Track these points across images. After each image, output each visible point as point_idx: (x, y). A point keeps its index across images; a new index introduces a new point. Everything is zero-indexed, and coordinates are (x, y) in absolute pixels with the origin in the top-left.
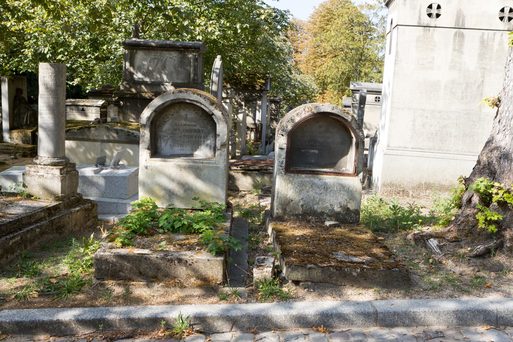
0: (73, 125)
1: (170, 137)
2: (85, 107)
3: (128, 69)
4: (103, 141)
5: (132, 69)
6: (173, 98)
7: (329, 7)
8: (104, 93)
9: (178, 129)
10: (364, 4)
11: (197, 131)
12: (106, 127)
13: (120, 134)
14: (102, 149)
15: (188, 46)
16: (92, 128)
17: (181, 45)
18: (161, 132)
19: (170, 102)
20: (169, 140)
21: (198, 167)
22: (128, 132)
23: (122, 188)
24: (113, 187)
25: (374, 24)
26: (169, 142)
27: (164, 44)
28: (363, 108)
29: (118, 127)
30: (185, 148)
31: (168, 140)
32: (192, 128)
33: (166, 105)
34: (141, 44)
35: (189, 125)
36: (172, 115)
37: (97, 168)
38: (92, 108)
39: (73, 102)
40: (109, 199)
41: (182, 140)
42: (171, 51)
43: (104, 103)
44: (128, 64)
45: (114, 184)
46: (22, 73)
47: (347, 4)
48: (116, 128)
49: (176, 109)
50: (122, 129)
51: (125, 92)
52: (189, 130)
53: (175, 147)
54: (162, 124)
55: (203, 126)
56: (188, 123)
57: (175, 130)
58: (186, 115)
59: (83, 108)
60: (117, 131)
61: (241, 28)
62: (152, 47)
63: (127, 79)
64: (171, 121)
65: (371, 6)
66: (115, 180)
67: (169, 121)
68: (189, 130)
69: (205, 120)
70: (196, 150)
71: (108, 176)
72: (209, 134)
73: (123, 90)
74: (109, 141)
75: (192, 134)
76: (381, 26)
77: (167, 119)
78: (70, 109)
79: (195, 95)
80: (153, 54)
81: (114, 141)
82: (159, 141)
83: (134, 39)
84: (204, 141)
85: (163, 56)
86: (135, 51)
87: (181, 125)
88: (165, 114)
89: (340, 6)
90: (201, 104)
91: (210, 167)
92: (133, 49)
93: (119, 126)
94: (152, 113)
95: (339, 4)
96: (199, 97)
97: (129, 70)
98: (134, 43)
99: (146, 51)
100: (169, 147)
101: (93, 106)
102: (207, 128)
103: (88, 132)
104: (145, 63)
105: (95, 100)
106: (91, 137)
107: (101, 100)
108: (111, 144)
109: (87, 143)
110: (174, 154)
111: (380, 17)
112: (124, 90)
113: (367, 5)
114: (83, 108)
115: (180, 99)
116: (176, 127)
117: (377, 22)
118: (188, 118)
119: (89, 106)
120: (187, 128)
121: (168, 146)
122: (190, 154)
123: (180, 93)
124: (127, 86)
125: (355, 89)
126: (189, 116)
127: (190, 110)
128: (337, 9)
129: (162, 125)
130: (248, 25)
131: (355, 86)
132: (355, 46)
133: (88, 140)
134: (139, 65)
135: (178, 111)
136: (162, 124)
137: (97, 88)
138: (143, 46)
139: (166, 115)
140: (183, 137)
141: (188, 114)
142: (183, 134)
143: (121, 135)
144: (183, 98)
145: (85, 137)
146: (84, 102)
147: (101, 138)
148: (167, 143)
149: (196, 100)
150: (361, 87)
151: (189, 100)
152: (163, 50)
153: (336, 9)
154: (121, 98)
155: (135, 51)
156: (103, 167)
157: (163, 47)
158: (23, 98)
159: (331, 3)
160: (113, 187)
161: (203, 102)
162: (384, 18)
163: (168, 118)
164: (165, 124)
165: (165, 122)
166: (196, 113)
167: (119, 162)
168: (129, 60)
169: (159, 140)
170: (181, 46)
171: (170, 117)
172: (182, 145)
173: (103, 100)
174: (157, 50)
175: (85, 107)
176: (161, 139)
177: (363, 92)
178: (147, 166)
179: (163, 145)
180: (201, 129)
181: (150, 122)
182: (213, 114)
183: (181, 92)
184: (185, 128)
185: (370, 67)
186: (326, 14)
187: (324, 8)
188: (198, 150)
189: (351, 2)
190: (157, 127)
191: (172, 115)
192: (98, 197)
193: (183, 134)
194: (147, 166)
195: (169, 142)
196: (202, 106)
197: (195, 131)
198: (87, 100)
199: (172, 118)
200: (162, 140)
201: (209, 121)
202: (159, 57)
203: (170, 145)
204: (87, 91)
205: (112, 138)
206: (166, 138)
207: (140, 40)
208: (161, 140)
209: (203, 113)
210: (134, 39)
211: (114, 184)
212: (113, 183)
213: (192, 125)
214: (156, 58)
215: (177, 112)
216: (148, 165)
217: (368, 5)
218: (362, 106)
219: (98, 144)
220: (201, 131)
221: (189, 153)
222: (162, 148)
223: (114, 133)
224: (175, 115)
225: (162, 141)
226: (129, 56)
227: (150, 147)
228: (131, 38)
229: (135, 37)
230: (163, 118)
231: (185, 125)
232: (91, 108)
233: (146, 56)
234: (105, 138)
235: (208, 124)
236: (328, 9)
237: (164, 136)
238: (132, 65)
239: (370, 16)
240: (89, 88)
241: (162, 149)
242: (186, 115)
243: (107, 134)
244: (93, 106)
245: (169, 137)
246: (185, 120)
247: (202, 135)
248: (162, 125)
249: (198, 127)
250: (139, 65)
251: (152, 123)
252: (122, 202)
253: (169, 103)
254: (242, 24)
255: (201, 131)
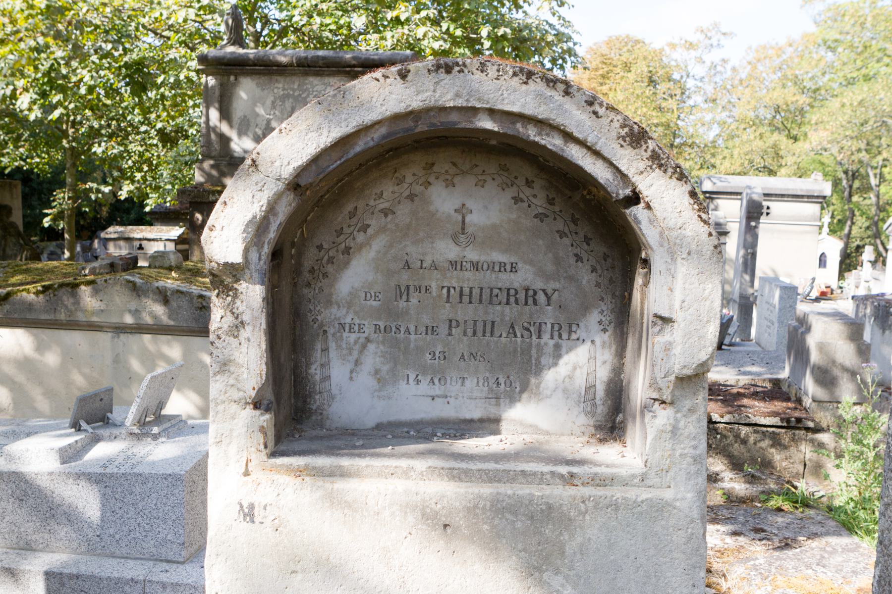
0: (29, 279)
1: (377, 328)
2: (144, 243)
3: (216, 126)
4: (120, 329)
5: (225, 128)
6: (400, 108)
7: (604, 53)
8: (183, 214)
9: (418, 289)
10: (676, 41)
11: (522, 296)
12: (129, 281)
13: (174, 304)
14: (118, 355)
15: (373, 60)
16: (83, 287)
17: (354, 58)
18: (329, 303)
19: (383, 130)
20: (371, 347)
21: (550, 507)
22: (201, 296)
23: (165, 520)
24: (131, 513)
25: (696, 77)
26: (372, 358)
27: (310, 56)
28: (756, 227)
29: (171, 282)
30: (454, 388)
31: (364, 347)
32: (490, 278)
33: (359, 146)
34: (249, 59)
35: (476, 266)
36: (385, 212)
37: (77, 438)
38: (160, 242)
39: (121, 232)
40: (114, 562)
41: (439, 349)
42: (329, 75)
43: (183, 233)
44: (214, 114)
45: (135, 505)
46: (9, 173)
47: (638, 46)
48: (161, 284)
49: (409, 179)
50: (184, 287)
51: (208, 187)
52: (476, 292)
53: (402, 384)
54: (331, 261)
55: (550, 267)
56: (472, 255)
57: (404, 292)
58: (462, 210)
59: (141, 245)
60: (164, 297)
61: (492, 37)
62: (279, 65)
63: (213, 154)
64: (378, 244)
65: (691, 44)
66: (138, 490)
67: (367, 243)
68: (476, 292)
69: (562, 234)
70: (513, 399)
71: (112, 475)
72: (585, 309)
73: (201, 184)
74: (139, 329)
75: (496, 312)
76: (710, 81)
77: (361, 237)
78: (115, 246)
79: (532, 86)
80: (281, 85)
81: (158, 329)
82: (318, 354)
83: (231, 49)
84: (557, 347)
85: (307, 89)
86: (232, 78)
87: (435, 266)
88: (349, 207)
89: (625, 49)
90: (568, 137)
91: (615, 506)
92: (229, 75)
93: (174, 278)
94: (278, 197)
95: (623, 46)
96: (557, 96)
97: (218, 130)
98: (229, 56)
99: (264, 79)
100: (372, 382)
101: (161, 240)
102: (571, 279)
103: (71, 300)
104: (260, 110)
105: (164, 228)
106: (81, 317)
107: (177, 228)
108: (147, 338)
109: (77, 339)
110: (392, 418)
111: (708, 64)
112: (205, 183)
113: (683, 42)
114: (141, 245)
115: (443, 109)
116: (405, 278)
117: (703, 74)
118: (469, 230)
119: (153, 240)
120: (469, 279)
121: (365, 379)
122: (481, 420)
123: (442, 74)
124: (214, 173)
125: (715, 190)
126: (476, 219)
127: (481, 184)
128: (620, 55)
129: (330, 269)
130: (508, 31)
131: (715, 184)
132: (664, 120)
133: (72, 325)
134: (245, 117)
135: (418, 189)
136: (331, 261)
137: (168, 204)
138: (255, 65)
139: (352, 215)
140: (443, 330)
141: (470, 204)
142: (446, 312)
143: (179, 307)
144: (460, 102)
145: (62, 316)
146: (142, 231)
147: (114, 320)
148: (357, 363)
149: (542, 112)
150: (729, 185)
151: (492, 112)
152: (306, 74)
153: (617, 55)
154: (196, 203)
155: (232, 78)
156: (101, 432)
157: (309, 66)
158: (13, 225)
159: (608, 44)
160: (131, 513)
161: (579, 124)
162: (715, 66)
163: (365, 228)
164: (347, 264)
165: (347, 251)
166: (517, 200)
167: (161, 405)
168: (217, 105)
169: (319, 346)
170: (354, 62)
171: (374, 223)
172: (438, 375)
173: (181, 227)
174: (293, 74)
175: (144, 243)
176: (325, 341)
177: (754, 193)
178: (252, 507)
179: (338, 371)
180: (539, 284)
181: (266, 250)
182: (635, 199)
183: (448, 70)
184: (454, 280)
185: (693, 159)
186: (600, 65)
187: (596, 54)
188: (525, 396)
189: (644, 43)
190: (307, 276)
191: (385, 212)
192: (74, 551)
193: (446, 312)
194: (252, 507)
195: (372, 358)
196: (576, 155)
197: (510, 295)
198: (148, 228)
199: (383, 230)
200: (332, 345)
201: (587, 240)
202: (296, 94)
203: (377, 372)
204: (147, 209)
205: (149, 320)
206: (353, 337)
207: (245, 51)
208: (325, 350)
209: (551, 202)
210: (231, 49)
211: (135, 505)
212: (129, 499)
213: (491, 266)
214: (287, 96)
215: (412, 197)
216: (259, 499)
217: (686, 42)
218: (753, 224)
219: (104, 339)
220: (541, 298)
221: (476, 414)
222: (335, 391)
223: (155, 301)
224: (404, 212)
225: (333, 353)
226: (217, 93)
227: (269, 395)
228: (223, 47)
229: (233, 44)
230: (340, 232)
231: (453, 264)
232: (156, 243)
233: (263, 90)
234: (129, 320)
235: (579, 258)
236: (603, 56)
237: (342, 326)
238: (225, 115)
239: (689, 62)
240: (151, 204)
241: (333, 397)
242: (462, 210)
243: (133, 305)
244: (161, 240)
245: (368, 329)
246: (455, 239)
247: (549, 316)
248: (330, 269)
249: (525, 276)
250: (245, 117)
251: (276, 254)
252: (164, 577)
253: (377, 134)
254: (494, 28)
255: (541, 298)
